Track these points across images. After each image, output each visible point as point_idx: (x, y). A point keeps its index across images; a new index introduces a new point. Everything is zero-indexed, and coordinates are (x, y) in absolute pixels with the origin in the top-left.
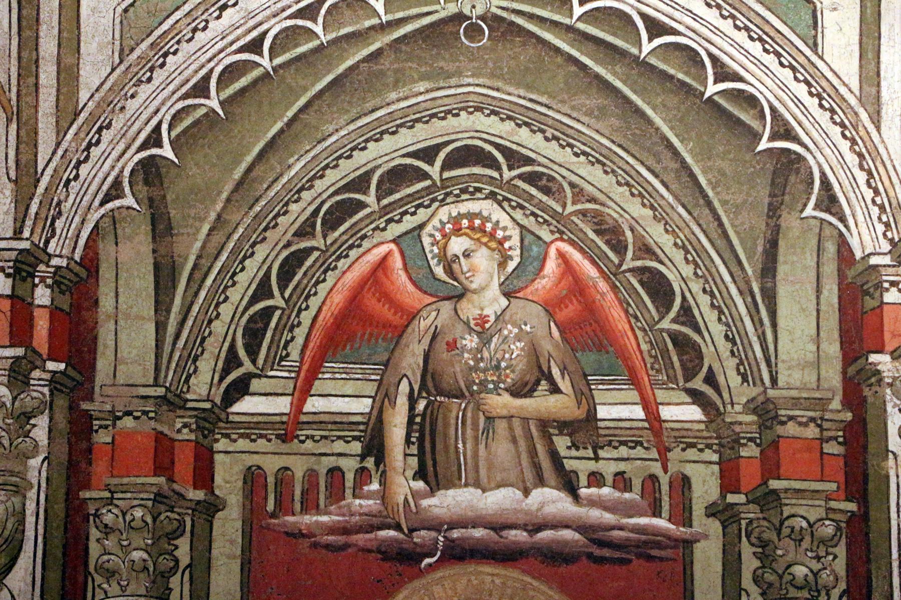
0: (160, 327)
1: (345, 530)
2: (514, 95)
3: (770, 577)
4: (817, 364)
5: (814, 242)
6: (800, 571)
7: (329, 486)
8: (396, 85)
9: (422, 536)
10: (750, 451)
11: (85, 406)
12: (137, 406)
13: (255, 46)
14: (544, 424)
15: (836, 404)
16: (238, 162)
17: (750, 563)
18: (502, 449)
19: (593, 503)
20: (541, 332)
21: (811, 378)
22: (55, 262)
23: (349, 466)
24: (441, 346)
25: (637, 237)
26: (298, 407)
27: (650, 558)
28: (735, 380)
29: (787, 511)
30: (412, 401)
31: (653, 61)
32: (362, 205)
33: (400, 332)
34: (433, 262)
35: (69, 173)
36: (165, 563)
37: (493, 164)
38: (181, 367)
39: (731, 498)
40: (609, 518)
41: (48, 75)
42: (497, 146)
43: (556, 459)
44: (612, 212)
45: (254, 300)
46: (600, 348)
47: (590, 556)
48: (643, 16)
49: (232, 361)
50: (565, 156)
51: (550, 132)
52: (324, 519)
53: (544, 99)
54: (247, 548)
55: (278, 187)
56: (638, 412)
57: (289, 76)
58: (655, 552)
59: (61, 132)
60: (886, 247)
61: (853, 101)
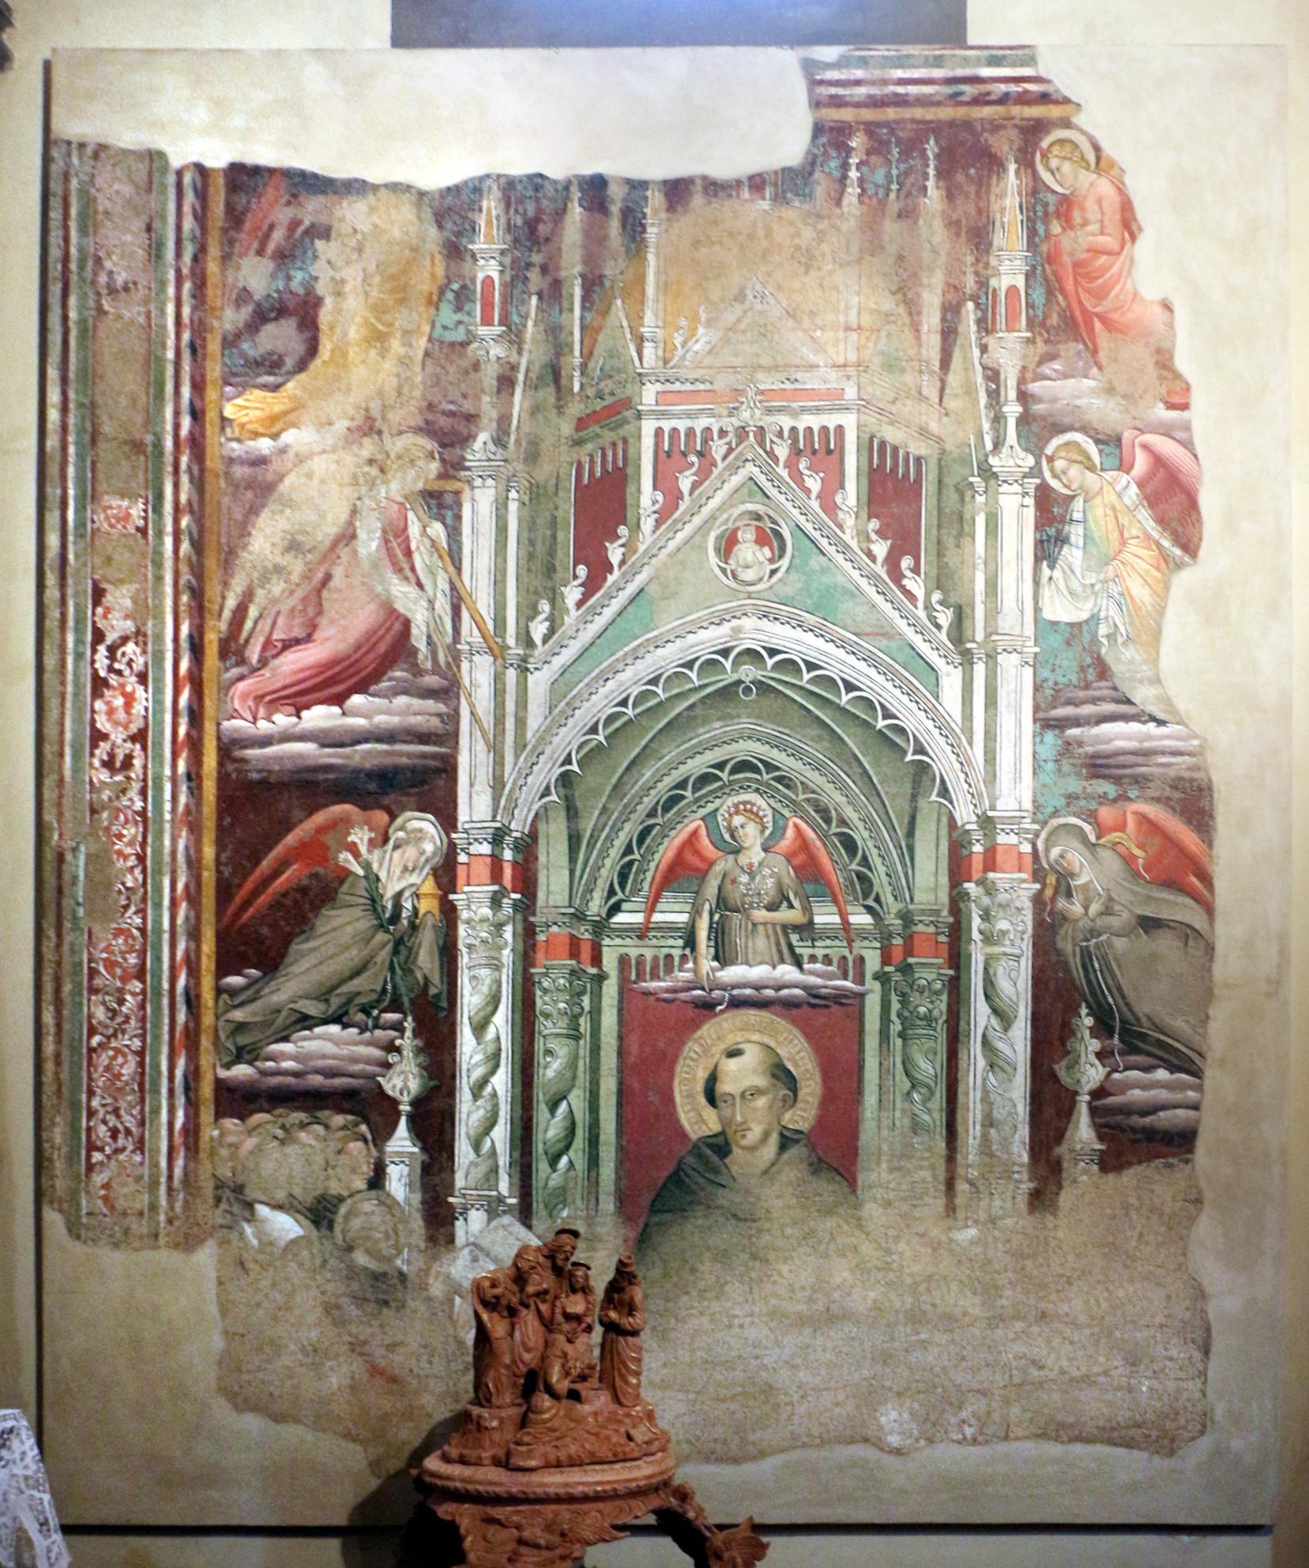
0: (572, 872)
1: (674, 991)
2: (769, 729)
3: (906, 1014)
4: (935, 890)
5: (935, 817)
6: (922, 1010)
7: (665, 965)
8: (704, 723)
9: (716, 994)
10: (898, 941)
11: (532, 919)
12: (560, 919)
13: (624, 703)
14: (784, 927)
15: (945, 913)
16: (613, 773)
17: (895, 1006)
18: (761, 943)
19: (811, 973)
20: (784, 873)
21: (932, 898)
22: (515, 834)
23: (676, 953)
24: (728, 881)
25: (838, 814)
26: (648, 920)
27: (842, 1004)
28: (891, 899)
29: (917, 975)
30: (711, 915)
31: (848, 707)
32: (683, 797)
33: (705, 873)
34: (723, 831)
35: (521, 782)
36: (577, 1010)
37: (756, 770)
38: (583, 896)
39: (887, 969)
40: (819, 981)
41: (510, 724)
42: (760, 760)
43: (791, 947)
44: (824, 799)
45: (624, 855)
46: (816, 881)
47: (809, 1004)
48: (843, 680)
49: (612, 892)
50: (798, 765)
51: (790, 751)
52: (663, 984)
53: (787, 731)
54: (621, 1000)
55: (637, 787)
56: (837, 919)
57: (644, 721)
58: (844, 1001)
59: (517, 757)
60: (974, 819)
61: (958, 731)
